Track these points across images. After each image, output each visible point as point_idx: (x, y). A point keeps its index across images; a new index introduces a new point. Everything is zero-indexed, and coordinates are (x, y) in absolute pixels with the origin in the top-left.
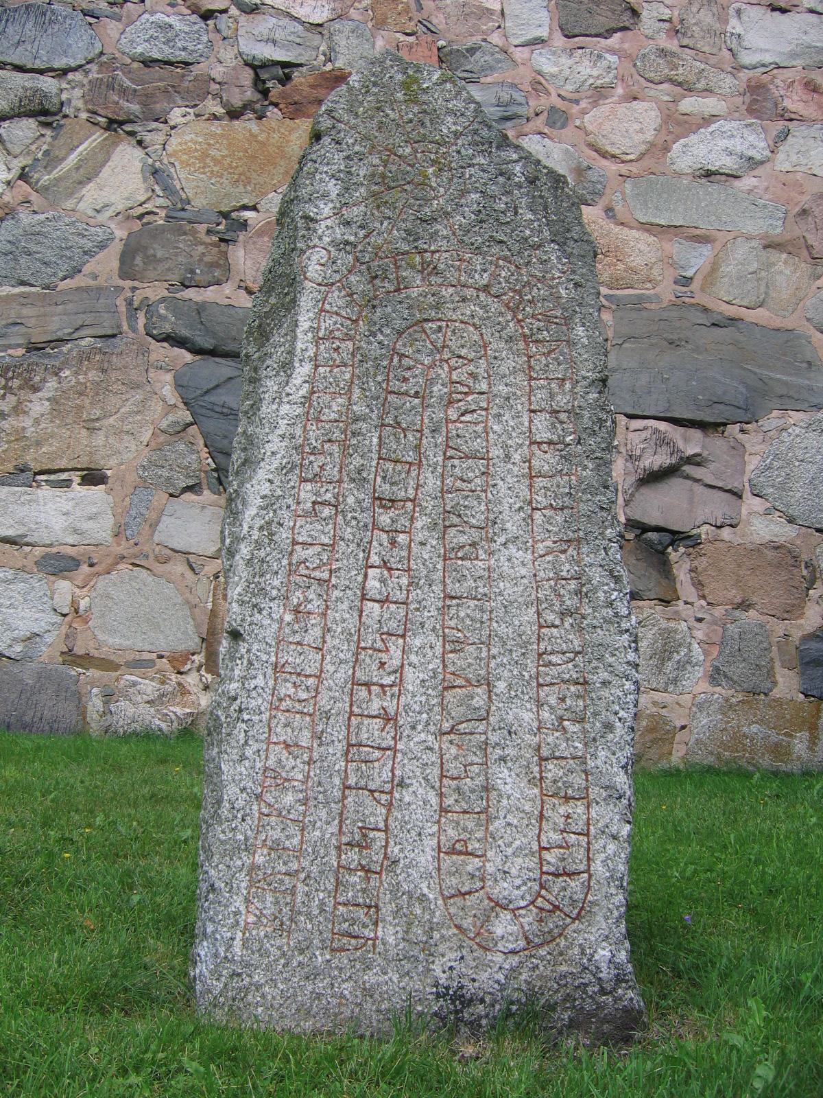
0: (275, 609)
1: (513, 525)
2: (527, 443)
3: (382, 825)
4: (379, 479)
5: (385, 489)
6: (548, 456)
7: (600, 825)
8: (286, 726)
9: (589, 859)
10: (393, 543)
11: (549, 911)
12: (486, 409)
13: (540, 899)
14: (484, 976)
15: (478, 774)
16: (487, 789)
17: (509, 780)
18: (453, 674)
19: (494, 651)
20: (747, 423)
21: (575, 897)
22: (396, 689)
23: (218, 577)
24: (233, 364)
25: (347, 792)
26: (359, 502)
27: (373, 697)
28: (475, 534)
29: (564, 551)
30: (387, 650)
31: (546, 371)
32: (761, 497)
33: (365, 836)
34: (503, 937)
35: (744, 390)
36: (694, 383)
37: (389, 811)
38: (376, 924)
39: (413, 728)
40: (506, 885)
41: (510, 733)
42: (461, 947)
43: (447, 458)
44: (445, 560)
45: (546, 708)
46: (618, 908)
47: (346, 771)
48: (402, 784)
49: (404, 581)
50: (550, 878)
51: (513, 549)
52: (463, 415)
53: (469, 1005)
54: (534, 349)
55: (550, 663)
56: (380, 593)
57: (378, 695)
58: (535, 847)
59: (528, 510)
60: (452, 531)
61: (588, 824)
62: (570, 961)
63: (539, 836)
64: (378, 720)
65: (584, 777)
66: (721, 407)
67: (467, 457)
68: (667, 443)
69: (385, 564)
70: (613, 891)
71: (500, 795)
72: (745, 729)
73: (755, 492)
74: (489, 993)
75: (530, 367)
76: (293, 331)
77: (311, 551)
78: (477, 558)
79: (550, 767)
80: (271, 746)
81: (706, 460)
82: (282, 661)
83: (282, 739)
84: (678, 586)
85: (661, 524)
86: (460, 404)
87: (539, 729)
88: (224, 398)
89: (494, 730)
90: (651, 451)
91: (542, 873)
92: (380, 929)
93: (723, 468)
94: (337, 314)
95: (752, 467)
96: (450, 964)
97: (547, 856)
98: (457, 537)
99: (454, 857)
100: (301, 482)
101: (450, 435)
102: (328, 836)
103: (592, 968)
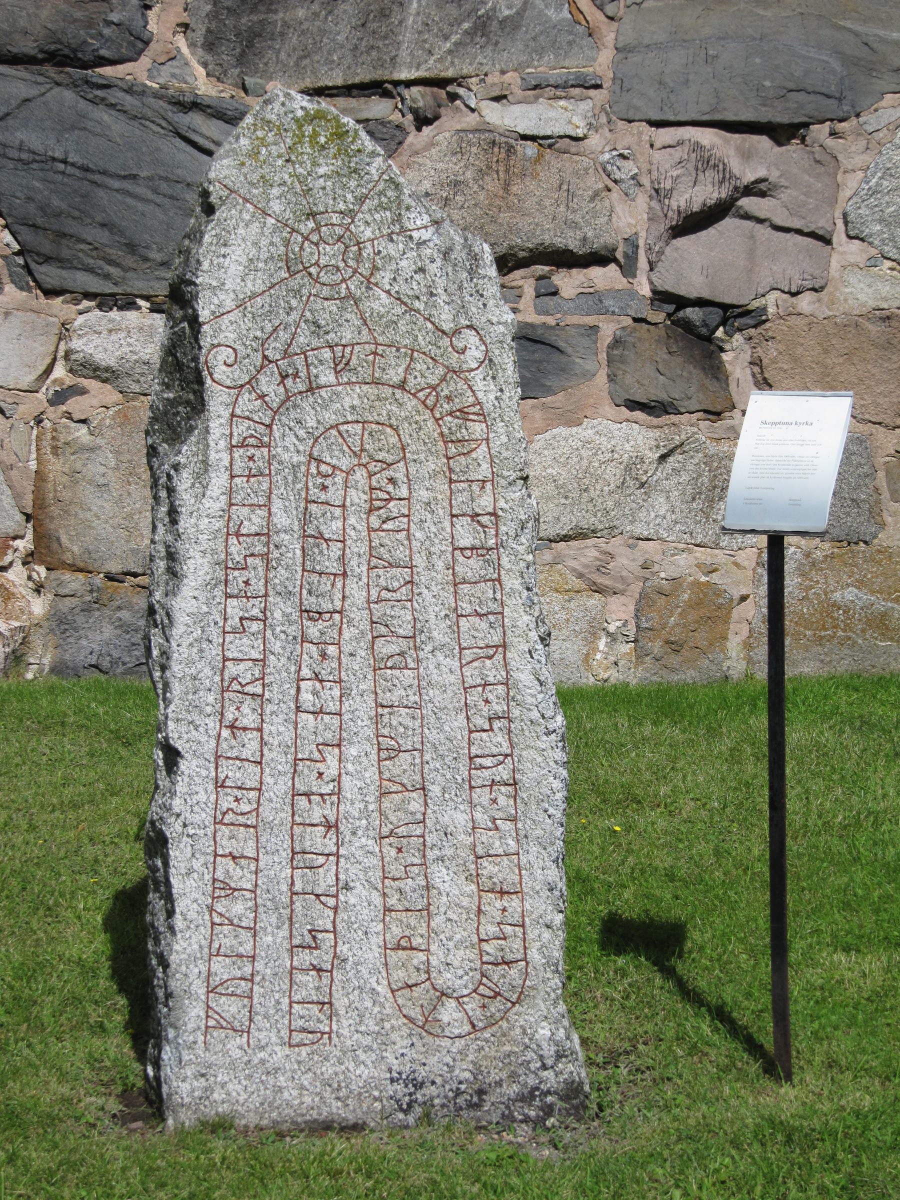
0: (211, 725)
1: (440, 633)
2: (450, 549)
3: (330, 927)
4: (305, 592)
5: (310, 602)
6: (471, 561)
7: (534, 916)
8: (230, 838)
9: (525, 948)
10: (324, 655)
11: (490, 997)
12: (408, 516)
13: (482, 987)
14: (432, 1060)
15: (418, 875)
16: (428, 888)
17: (447, 878)
18: (389, 780)
19: (427, 757)
20: (841, 120)
21: (514, 983)
22: (335, 798)
23: (41, 421)
24: (27, 75)
25: (295, 897)
26: (284, 615)
27: (315, 806)
28: (404, 643)
29: (490, 658)
30: (324, 760)
31: (466, 473)
32: (862, 240)
33: (314, 938)
34: (449, 1024)
35: (836, 65)
36: (758, 60)
37: (336, 913)
38: (330, 1018)
39: (354, 833)
40: (449, 976)
41: (446, 834)
42: (410, 1035)
43: (370, 568)
44: (375, 670)
45: (479, 808)
46: (554, 991)
47: (292, 877)
48: (347, 887)
49: (336, 692)
50: (490, 967)
51: (440, 657)
52: (384, 522)
53: (421, 1087)
54: (454, 450)
55: (482, 767)
56: (314, 705)
57: (318, 804)
58: (475, 939)
59: (453, 616)
60: (380, 642)
61: (523, 916)
62: (514, 1041)
63: (478, 930)
64: (320, 828)
65: (517, 871)
66: (801, 96)
67: (391, 565)
68: (715, 166)
69: (317, 677)
70: (549, 975)
71: (440, 893)
72: (837, 596)
73: (851, 233)
74: (440, 1075)
75: (451, 470)
76: (205, 439)
77: (242, 666)
78: (406, 668)
79: (485, 864)
80: (218, 858)
81: (776, 187)
82: (222, 776)
83: (227, 851)
84: (733, 387)
85: (706, 294)
86: (382, 511)
87: (474, 828)
88: (21, 135)
89: (430, 832)
90: (688, 180)
91: (483, 963)
92: (334, 1023)
93: (802, 197)
94: (248, 418)
95: (848, 193)
96: (401, 1051)
97: (485, 946)
98: (385, 648)
99: (400, 952)
100: (227, 597)
101: (373, 544)
102: (278, 941)
103: (534, 1046)
